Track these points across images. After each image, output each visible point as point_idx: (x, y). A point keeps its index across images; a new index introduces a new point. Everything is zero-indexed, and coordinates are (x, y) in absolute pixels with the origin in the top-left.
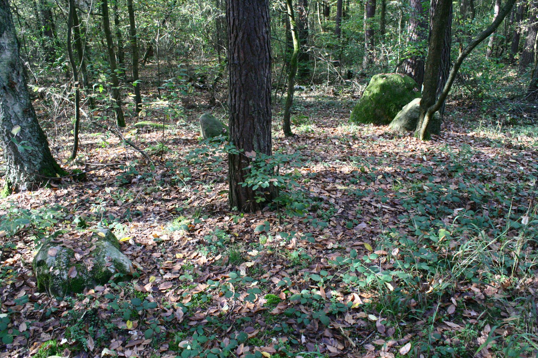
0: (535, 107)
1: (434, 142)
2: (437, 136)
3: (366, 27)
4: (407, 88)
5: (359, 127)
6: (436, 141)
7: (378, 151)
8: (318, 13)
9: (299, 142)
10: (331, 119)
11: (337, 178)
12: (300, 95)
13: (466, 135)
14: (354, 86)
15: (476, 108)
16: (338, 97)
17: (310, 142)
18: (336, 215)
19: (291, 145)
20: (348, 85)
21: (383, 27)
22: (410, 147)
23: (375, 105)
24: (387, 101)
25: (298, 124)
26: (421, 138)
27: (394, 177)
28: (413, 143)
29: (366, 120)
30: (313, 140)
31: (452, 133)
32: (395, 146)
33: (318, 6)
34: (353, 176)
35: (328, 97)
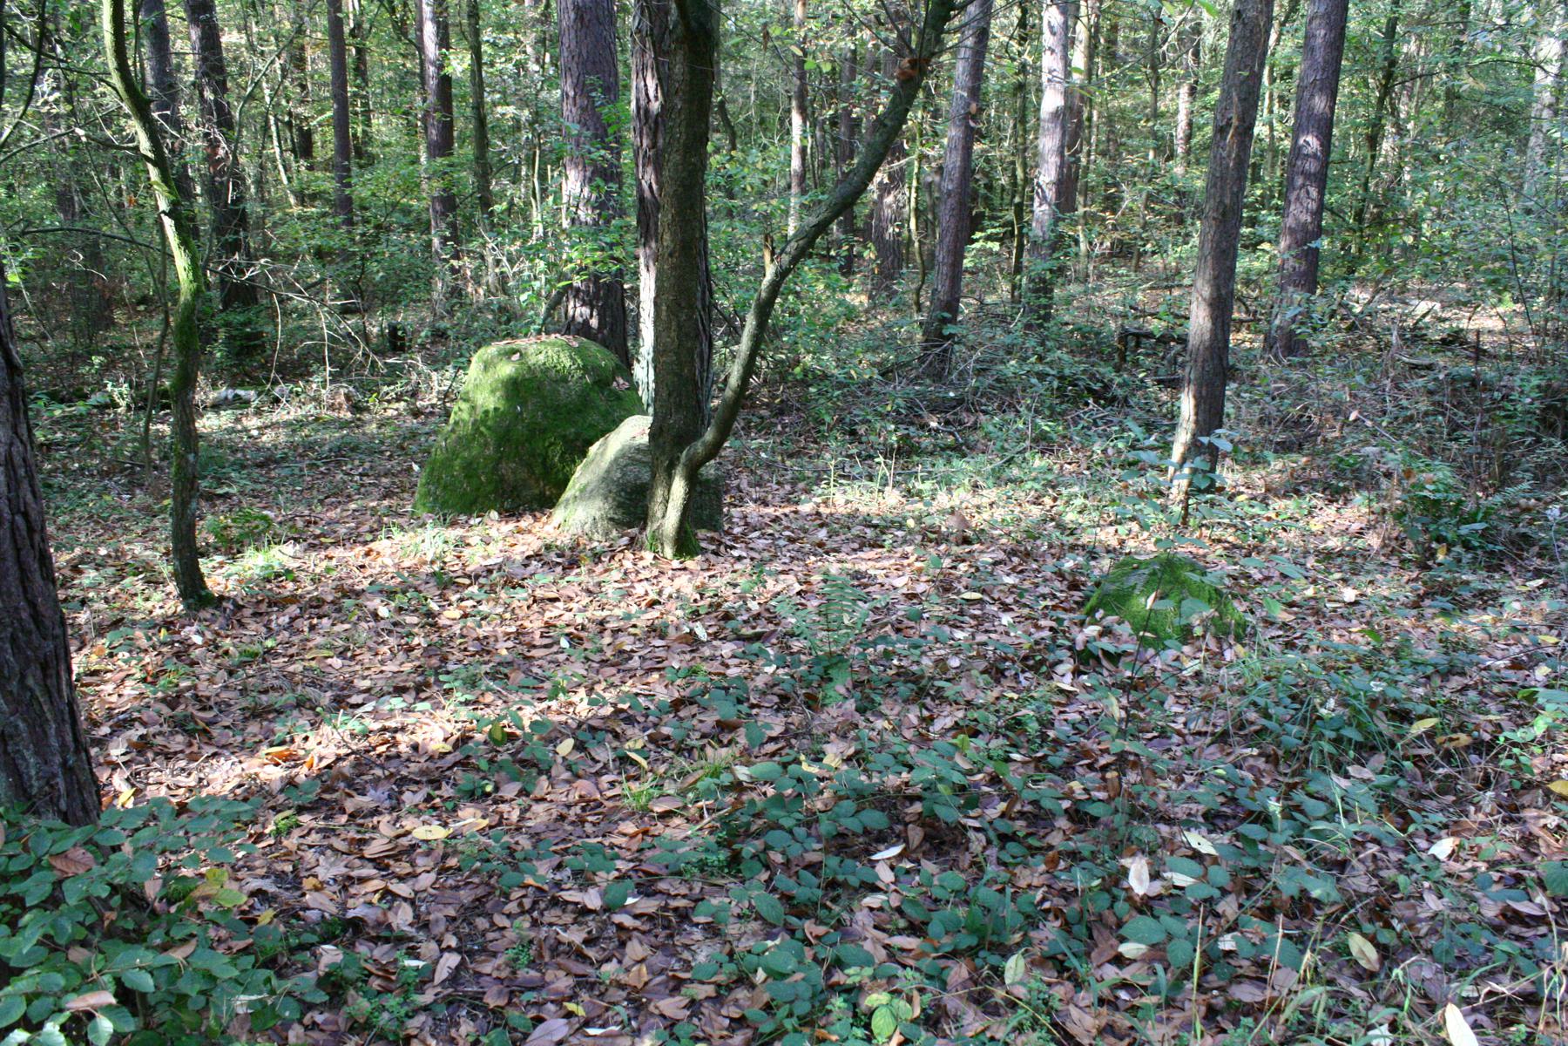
0: (952, 394)
1: (712, 557)
2: (715, 535)
3: (432, 188)
4: (595, 383)
5: (453, 534)
6: (716, 553)
7: (535, 625)
8: (277, 150)
9: (242, 625)
10: (353, 506)
11: (403, 781)
12: (238, 420)
13: (796, 512)
14: (414, 377)
15: (801, 414)
16: (366, 417)
17: (284, 620)
18: (427, 998)
19: (212, 645)
20: (394, 374)
21: (484, 186)
22: (640, 589)
24: (536, 432)
25: (232, 548)
26: (669, 551)
27: (617, 736)
28: (645, 574)
29: (474, 503)
30: (293, 609)
31: (751, 508)
32: (589, 592)
33: (273, 128)
34: (464, 764)
35: (333, 421)
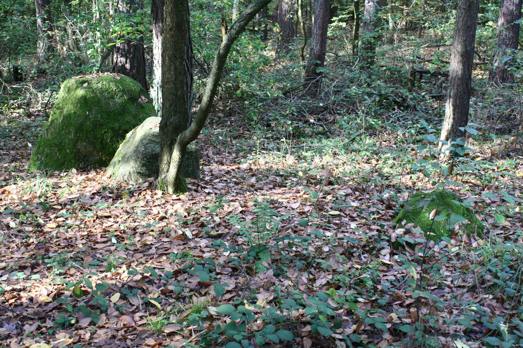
0: (321, 105)
1: (194, 193)
4: (129, 99)
5: (51, 181)
6: (196, 191)
7: (98, 230)
11: (24, 319)
13: (239, 168)
14: (28, 95)
15: (242, 114)
20: (17, 93)
22: (155, 211)
23: (76, 136)
24: (97, 125)
26: (171, 190)
27: (144, 291)
29: (63, 164)
31: (214, 166)
32: (127, 212)
34: (59, 308)
